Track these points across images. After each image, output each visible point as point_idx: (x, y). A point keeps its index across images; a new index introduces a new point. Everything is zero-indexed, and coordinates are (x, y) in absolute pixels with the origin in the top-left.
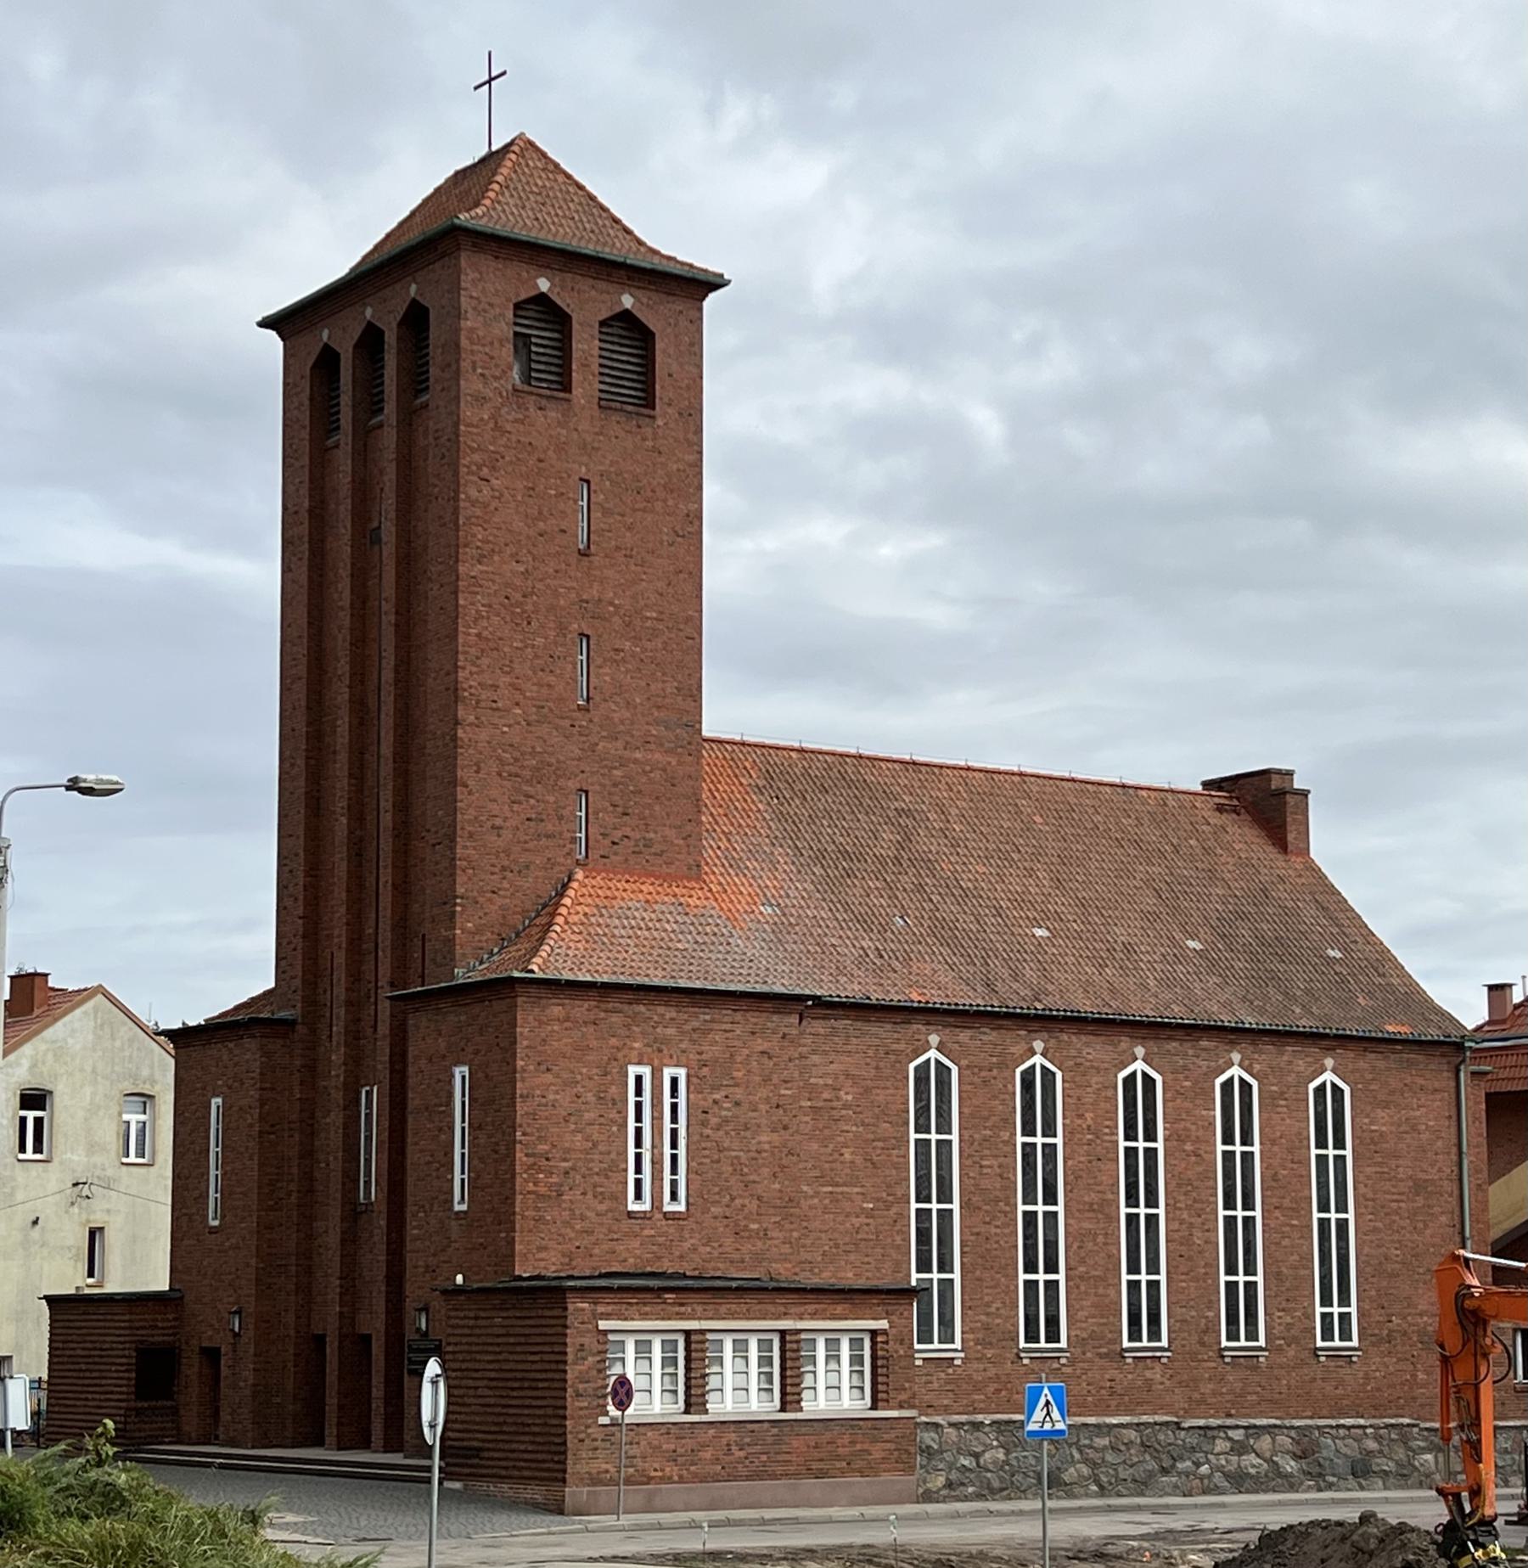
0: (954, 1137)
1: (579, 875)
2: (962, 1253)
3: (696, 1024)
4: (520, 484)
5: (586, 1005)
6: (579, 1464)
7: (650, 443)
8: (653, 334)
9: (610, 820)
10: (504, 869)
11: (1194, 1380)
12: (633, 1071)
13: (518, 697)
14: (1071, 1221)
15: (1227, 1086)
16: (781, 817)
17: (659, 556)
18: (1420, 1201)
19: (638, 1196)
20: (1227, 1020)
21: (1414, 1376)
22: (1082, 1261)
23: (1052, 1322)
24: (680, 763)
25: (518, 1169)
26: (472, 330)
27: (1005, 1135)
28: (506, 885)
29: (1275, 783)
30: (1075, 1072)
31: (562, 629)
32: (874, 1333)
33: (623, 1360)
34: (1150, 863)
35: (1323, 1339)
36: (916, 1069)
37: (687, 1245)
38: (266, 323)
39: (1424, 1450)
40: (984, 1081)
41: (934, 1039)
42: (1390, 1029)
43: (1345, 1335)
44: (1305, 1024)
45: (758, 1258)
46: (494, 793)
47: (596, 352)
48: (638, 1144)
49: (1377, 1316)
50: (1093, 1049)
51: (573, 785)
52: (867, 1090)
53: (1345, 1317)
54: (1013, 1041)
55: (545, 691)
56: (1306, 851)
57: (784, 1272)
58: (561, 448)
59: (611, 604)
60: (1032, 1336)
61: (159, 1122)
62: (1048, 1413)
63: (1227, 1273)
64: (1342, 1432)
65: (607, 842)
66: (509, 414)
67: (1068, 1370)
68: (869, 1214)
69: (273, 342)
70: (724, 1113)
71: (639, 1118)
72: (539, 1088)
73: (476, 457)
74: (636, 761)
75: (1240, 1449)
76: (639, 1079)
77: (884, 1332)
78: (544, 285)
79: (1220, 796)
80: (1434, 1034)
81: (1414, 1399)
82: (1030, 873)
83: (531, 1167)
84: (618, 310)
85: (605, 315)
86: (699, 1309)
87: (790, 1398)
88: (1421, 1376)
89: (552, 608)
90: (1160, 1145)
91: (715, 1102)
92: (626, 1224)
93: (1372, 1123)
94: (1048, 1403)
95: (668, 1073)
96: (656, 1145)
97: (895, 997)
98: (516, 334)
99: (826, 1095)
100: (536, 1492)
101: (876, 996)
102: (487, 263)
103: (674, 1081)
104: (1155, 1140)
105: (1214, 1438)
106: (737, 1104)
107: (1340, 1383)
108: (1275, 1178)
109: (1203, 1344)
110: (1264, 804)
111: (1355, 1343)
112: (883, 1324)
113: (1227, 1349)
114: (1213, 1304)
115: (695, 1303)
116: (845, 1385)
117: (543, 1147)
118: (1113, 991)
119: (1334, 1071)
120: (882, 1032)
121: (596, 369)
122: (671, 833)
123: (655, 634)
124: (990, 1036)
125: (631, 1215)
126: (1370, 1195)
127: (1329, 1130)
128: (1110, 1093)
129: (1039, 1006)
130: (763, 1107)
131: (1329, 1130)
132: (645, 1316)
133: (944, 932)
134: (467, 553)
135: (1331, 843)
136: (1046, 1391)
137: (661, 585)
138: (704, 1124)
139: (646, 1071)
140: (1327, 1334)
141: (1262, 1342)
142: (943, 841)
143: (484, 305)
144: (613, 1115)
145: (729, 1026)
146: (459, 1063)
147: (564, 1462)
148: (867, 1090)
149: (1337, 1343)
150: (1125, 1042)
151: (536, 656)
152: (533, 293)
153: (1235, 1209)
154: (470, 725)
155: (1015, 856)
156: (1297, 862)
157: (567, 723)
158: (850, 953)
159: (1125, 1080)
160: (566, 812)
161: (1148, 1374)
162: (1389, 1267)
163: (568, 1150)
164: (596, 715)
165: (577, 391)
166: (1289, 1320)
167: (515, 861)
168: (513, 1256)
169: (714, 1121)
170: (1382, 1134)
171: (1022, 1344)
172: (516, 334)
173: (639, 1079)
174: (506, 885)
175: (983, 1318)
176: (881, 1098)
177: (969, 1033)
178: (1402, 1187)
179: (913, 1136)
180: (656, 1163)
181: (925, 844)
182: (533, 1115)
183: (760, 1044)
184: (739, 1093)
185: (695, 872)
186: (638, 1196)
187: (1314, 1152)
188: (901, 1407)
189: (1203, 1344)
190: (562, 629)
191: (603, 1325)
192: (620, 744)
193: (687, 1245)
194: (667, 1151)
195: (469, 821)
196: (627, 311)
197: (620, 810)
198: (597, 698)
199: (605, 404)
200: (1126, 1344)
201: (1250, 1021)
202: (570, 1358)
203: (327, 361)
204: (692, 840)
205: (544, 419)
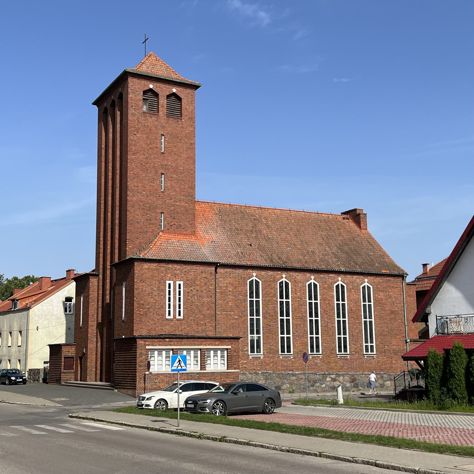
1: (161, 234)
2: (263, 329)
3: (186, 270)
4: (144, 136)
5: (154, 265)
6: (140, 384)
7: (180, 126)
8: (181, 99)
10: (140, 232)
11: (329, 362)
12: (168, 282)
13: (144, 189)
14: (294, 321)
15: (310, 285)
16: (221, 220)
17: (183, 154)
18: (393, 316)
19: (169, 315)
20: (336, 269)
21: (392, 362)
22: (297, 332)
23: (289, 347)
24: (189, 206)
25: (135, 307)
26: (131, 97)
27: (275, 299)
28: (140, 236)
29: (358, 212)
30: (295, 282)
31: (156, 172)
32: (227, 349)
33: (154, 357)
34: (322, 231)
35: (251, 353)
36: (250, 282)
37: (183, 327)
38: (94, 103)
39: (388, 380)
40: (268, 285)
41: (254, 274)
42: (383, 271)
43: (372, 351)
44: (359, 270)
46: (138, 213)
47: (166, 103)
48: (169, 301)
49: (381, 346)
50: (299, 276)
51: (159, 211)
52: (236, 287)
53: (372, 347)
55: (152, 187)
57: (211, 334)
58: (156, 127)
59: (170, 166)
60: (340, 351)
62: (180, 364)
63: (281, 334)
64: (363, 376)
65: (169, 225)
66: (142, 119)
67: (293, 360)
68: (236, 319)
69: (96, 108)
70: (193, 293)
71: (169, 294)
73: (133, 129)
74: (177, 205)
75: (334, 380)
76: (170, 284)
77: (230, 349)
80: (396, 273)
81: (392, 367)
82: (288, 234)
83: (138, 307)
84: (171, 92)
85: (168, 94)
86: (176, 343)
87: (203, 367)
88: (394, 361)
89: (154, 167)
90: (319, 301)
91: (191, 290)
92: (165, 322)
93: (379, 296)
94: (179, 361)
95: (178, 283)
98: (144, 99)
99: (224, 288)
100: (130, 392)
101: (238, 263)
102: (135, 80)
103: (180, 285)
104: (317, 300)
105: (326, 377)
106: (197, 291)
107: (371, 363)
108: (351, 310)
109: (331, 353)
111: (375, 353)
112: (230, 347)
113: (339, 354)
115: (185, 341)
116: (219, 363)
117: (142, 302)
118: (306, 262)
119: (314, 279)
120: (240, 271)
121: (165, 107)
124: (270, 273)
125: (167, 320)
126: (378, 314)
127: (366, 297)
128: (304, 288)
129: (284, 265)
130: (205, 291)
131: (366, 297)
132: (160, 345)
134: (129, 153)
135: (374, 227)
136: (179, 357)
137: (184, 161)
138: (188, 296)
139: (172, 283)
140: (367, 351)
141: (348, 353)
142: (265, 226)
143: (135, 88)
144: (162, 293)
145: (195, 271)
146: (124, 281)
147: (135, 384)
148: (236, 287)
149: (370, 353)
150: (308, 275)
151: (149, 179)
152: (148, 88)
153: (283, 316)
154: (131, 196)
155: (285, 230)
157: (158, 195)
159: (309, 285)
160: (158, 218)
161: (316, 361)
162: (384, 333)
163: (149, 303)
164: (166, 194)
165: (160, 113)
166: (356, 347)
167: (143, 231)
168: (133, 330)
169: (191, 295)
170: (382, 299)
171: (280, 353)
172: (144, 99)
173: (170, 284)
174: (140, 236)
175: (269, 346)
176: (240, 290)
177: (264, 272)
178: (388, 312)
179: (249, 299)
180: (175, 306)
181: (260, 227)
183: (204, 275)
184: (198, 288)
185: (194, 233)
186: (169, 315)
187: (362, 303)
188: (235, 369)
189: (331, 353)
190: (156, 172)
191: (147, 347)
192: (172, 201)
193: (183, 327)
194: (177, 303)
195: (131, 220)
196: (174, 93)
197: (173, 217)
198: (166, 189)
199: (168, 116)
200: (338, 353)
201: (343, 269)
202: (138, 356)
203: (106, 110)
204: (193, 226)
205: (151, 120)
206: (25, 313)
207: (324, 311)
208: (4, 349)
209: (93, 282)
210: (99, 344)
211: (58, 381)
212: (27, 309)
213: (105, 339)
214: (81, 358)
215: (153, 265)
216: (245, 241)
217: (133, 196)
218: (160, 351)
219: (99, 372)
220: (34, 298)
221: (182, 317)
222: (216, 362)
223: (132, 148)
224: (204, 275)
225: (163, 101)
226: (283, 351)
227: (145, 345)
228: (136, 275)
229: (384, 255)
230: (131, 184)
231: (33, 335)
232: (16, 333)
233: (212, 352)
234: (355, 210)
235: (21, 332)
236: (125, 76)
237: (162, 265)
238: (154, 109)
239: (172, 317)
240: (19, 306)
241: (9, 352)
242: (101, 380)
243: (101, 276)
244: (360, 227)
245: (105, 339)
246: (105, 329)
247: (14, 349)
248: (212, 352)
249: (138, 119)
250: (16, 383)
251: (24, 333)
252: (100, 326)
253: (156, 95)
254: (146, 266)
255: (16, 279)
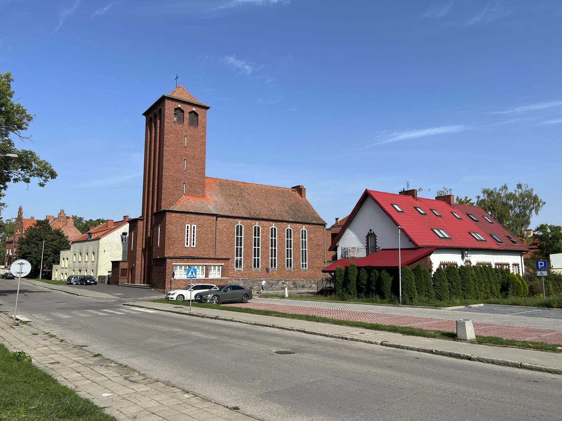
0: (243, 237)
6: (168, 286)
9: (189, 187)
12: (187, 225)
16: (221, 189)
20: (287, 220)
41: (240, 222)
43: (306, 267)
44: (300, 221)
45: (207, 254)
49: (311, 264)
51: (183, 182)
53: (306, 264)
54: (253, 222)
56: (305, 197)
60: (288, 267)
61: (538, 327)
66: (173, 125)
72: (169, 227)
75: (283, 283)
78: (179, 106)
79: (293, 189)
80: (320, 223)
87: (207, 275)
89: (180, 155)
95: (193, 226)
96: (191, 237)
97: (233, 215)
100: (161, 290)
101: (230, 215)
102: (170, 102)
110: (299, 189)
114: (284, 262)
120: (231, 220)
122: (200, 190)
123: (197, 160)
124: (249, 221)
127: (304, 236)
131: (304, 236)
133: (244, 207)
134: (165, 146)
135: (309, 196)
139: (189, 225)
140: (303, 267)
143: (169, 107)
150: (271, 223)
156: (303, 199)
158: (227, 209)
182: (169, 232)
183: (209, 221)
184: (205, 229)
185: (204, 196)
190: (181, 158)
201: (291, 220)
204: (203, 192)
205: (179, 126)
206: (97, 241)
207: (279, 244)
208: (83, 263)
209: (140, 224)
210: (143, 261)
211: (117, 283)
212: (98, 239)
213: (147, 259)
214: (131, 270)
215: (178, 215)
216: (235, 202)
217: (167, 172)
218: (181, 266)
219: (142, 278)
220: (103, 233)
221: (195, 246)
222: (181, 273)
223: (166, 143)
224: (209, 221)
225: (187, 115)
226: (255, 267)
227: (172, 263)
228: (167, 220)
229: (314, 212)
230: (165, 165)
231: (101, 256)
232: (90, 254)
233: (213, 267)
234: (299, 186)
235: (94, 253)
236: (163, 99)
237: (183, 214)
238: (181, 120)
239: (188, 246)
240: (93, 237)
241: (86, 265)
242: (144, 283)
243: (145, 220)
244: (302, 196)
245: (147, 259)
246: (147, 253)
247: (89, 264)
248: (213, 267)
249: (171, 125)
250: (90, 284)
251: (96, 254)
252: (144, 251)
253: (182, 111)
254: (173, 215)
255: (91, 220)
